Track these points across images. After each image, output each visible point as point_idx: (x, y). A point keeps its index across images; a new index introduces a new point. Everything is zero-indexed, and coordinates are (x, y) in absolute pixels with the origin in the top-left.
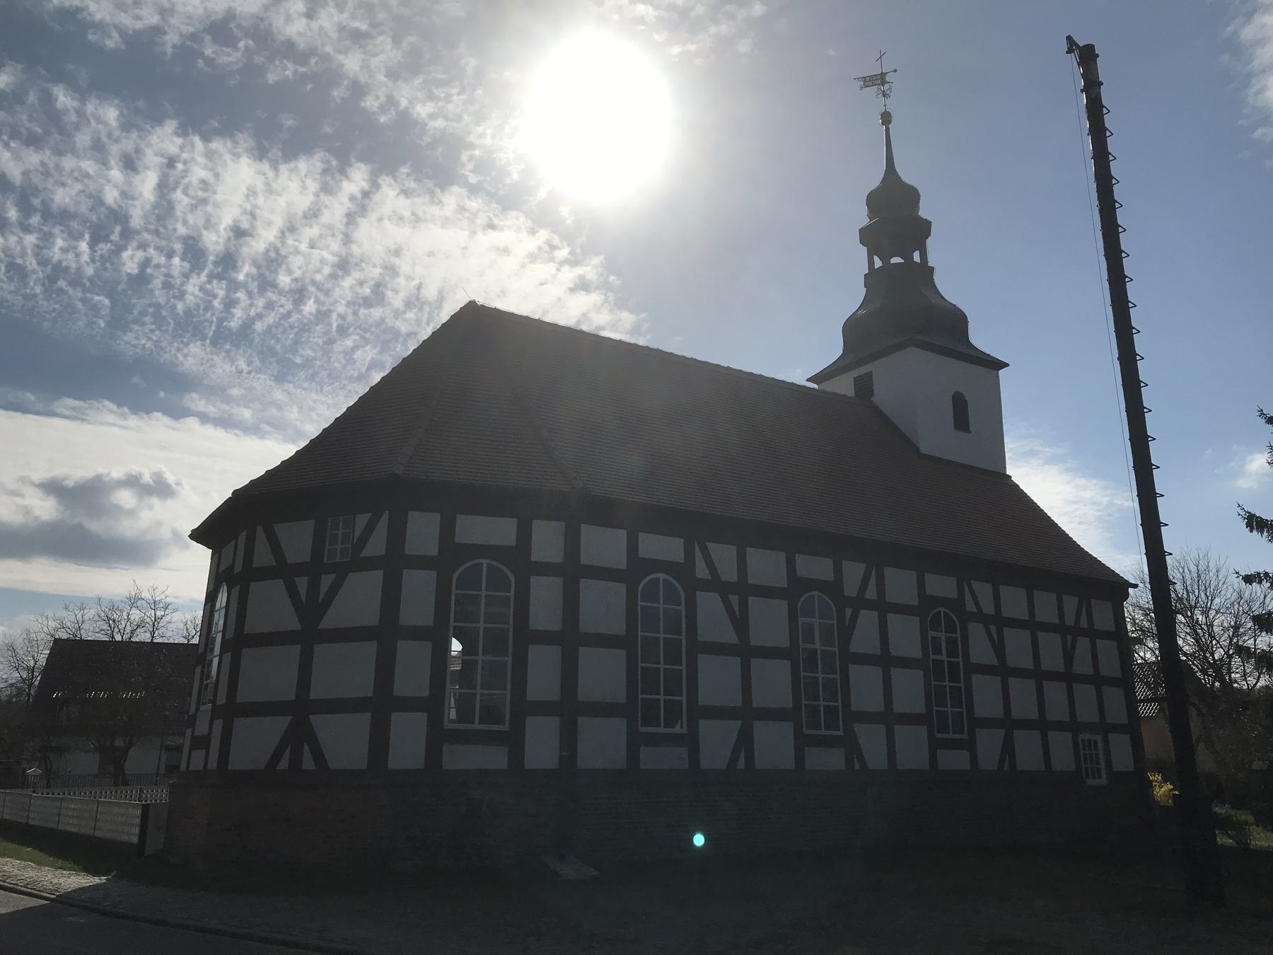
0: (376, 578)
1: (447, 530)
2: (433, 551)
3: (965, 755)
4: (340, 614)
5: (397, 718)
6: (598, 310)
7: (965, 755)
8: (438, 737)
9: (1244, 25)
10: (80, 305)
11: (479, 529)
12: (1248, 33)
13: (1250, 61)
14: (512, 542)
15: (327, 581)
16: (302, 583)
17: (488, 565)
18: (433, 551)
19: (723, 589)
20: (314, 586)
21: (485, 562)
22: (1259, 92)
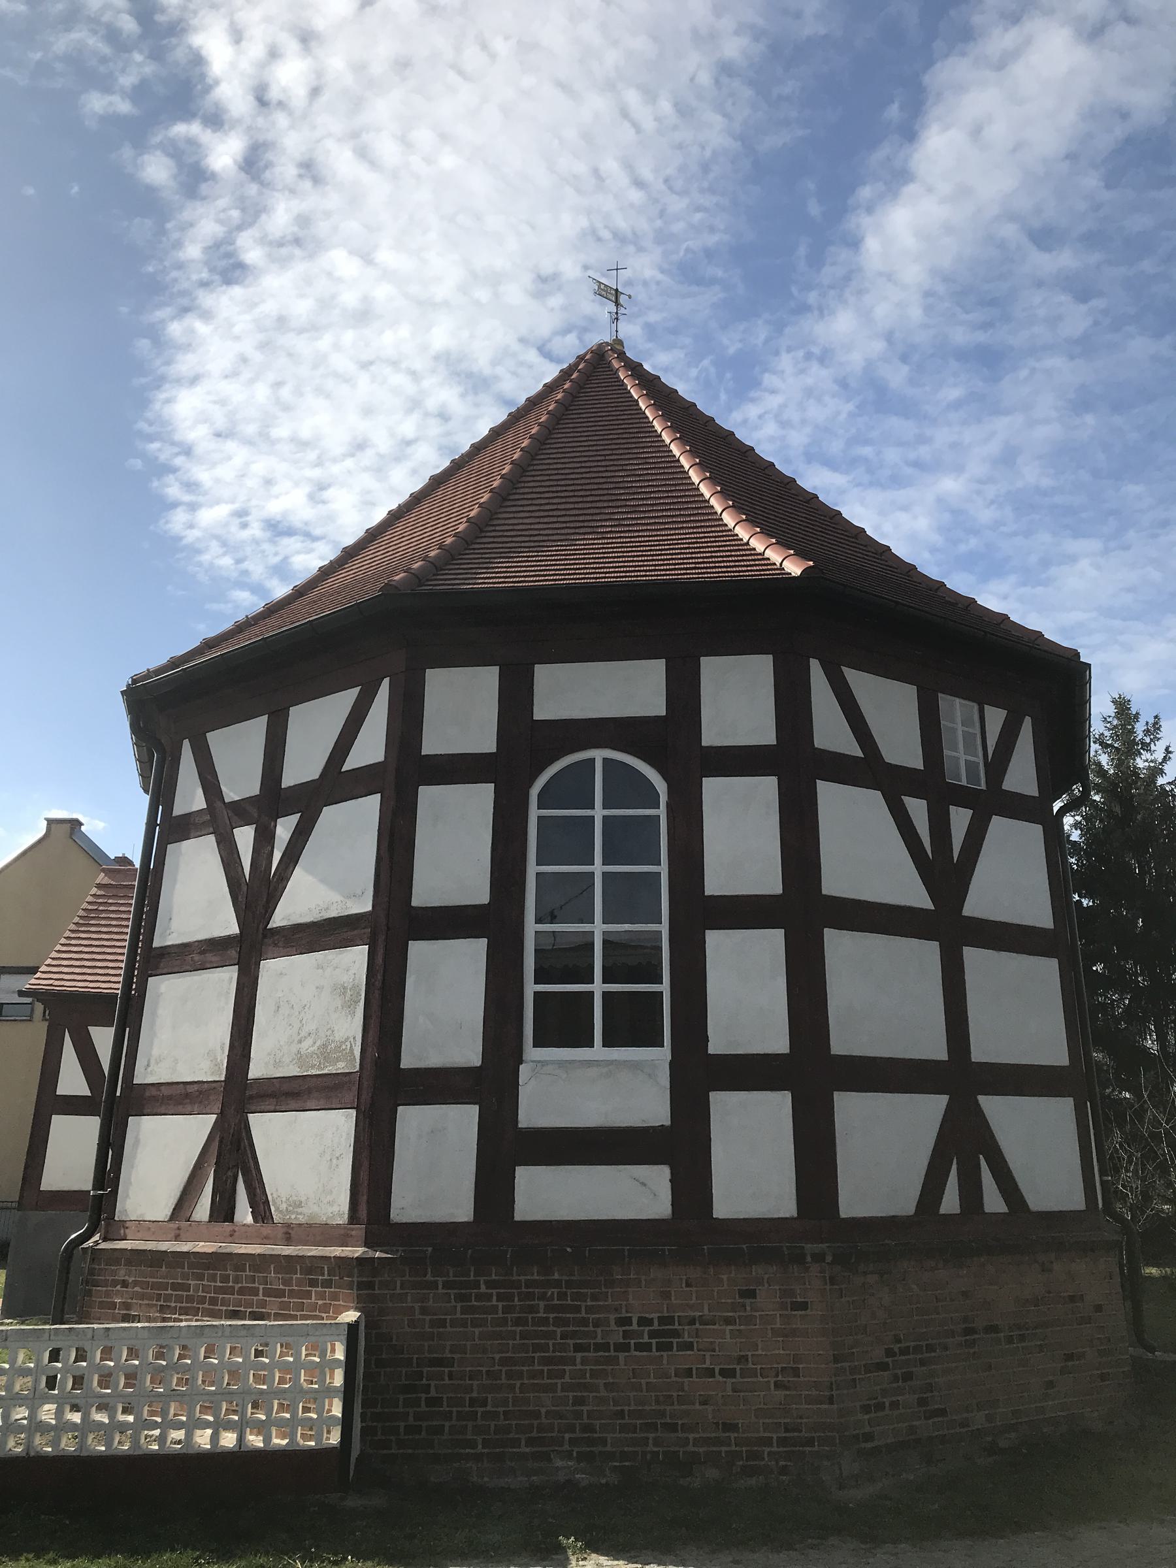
0: (365, 812)
1: (515, 697)
2: (485, 741)
3: (659, 1177)
4: (304, 899)
5: (774, 1039)
6: (160, 450)
7: (659, 1177)
8: (506, 1147)
9: (173, 318)
10: (500, 45)
11: (569, 691)
12: (175, 329)
13: (168, 363)
14: (658, 707)
15: (284, 829)
16: (245, 837)
17: (606, 761)
18: (485, 741)
19: (892, 783)
20: (265, 839)
21: (599, 755)
22: (168, 401)
